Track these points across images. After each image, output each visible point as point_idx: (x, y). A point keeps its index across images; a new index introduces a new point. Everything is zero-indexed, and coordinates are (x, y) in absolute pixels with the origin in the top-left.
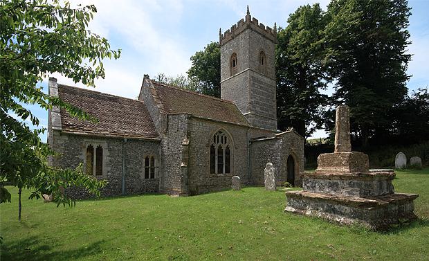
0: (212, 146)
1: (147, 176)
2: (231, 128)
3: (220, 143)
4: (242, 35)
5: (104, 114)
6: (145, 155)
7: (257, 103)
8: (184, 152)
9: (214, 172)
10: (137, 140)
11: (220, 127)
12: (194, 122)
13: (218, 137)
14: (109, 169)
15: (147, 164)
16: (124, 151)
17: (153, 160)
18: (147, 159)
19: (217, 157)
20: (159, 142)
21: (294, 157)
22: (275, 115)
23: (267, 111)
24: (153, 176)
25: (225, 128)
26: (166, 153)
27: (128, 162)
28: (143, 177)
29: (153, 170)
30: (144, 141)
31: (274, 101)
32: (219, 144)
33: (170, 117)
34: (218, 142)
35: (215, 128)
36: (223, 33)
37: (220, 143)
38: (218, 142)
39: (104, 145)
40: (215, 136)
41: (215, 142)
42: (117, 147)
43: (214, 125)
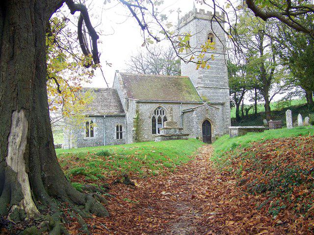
0: (154, 117)
1: (118, 138)
2: (166, 105)
3: (159, 115)
4: (192, 23)
5: (217, 207)
6: (116, 124)
7: (206, 77)
8: (134, 122)
9: (156, 133)
10: (111, 116)
11: (158, 105)
12: (140, 104)
13: (158, 111)
14: (97, 133)
15: (117, 130)
16: (104, 123)
17: (121, 127)
18: (117, 127)
19: (157, 124)
20: (124, 116)
21: (209, 121)
22: (227, 85)
23: (217, 81)
24: (121, 137)
25: (162, 105)
26: (128, 123)
27: (106, 129)
28: (115, 138)
29: (121, 134)
30: (115, 116)
31: (225, 73)
32: (158, 115)
33: (129, 101)
34: (158, 114)
35: (155, 106)
36: (180, 19)
37: (159, 115)
38: (158, 114)
39: (94, 121)
40: (155, 111)
41: (155, 114)
42: (100, 120)
43: (154, 105)
